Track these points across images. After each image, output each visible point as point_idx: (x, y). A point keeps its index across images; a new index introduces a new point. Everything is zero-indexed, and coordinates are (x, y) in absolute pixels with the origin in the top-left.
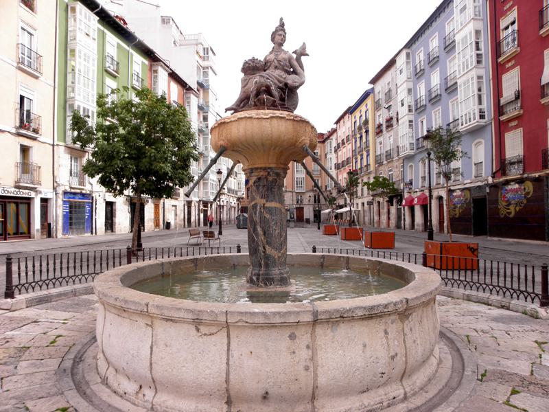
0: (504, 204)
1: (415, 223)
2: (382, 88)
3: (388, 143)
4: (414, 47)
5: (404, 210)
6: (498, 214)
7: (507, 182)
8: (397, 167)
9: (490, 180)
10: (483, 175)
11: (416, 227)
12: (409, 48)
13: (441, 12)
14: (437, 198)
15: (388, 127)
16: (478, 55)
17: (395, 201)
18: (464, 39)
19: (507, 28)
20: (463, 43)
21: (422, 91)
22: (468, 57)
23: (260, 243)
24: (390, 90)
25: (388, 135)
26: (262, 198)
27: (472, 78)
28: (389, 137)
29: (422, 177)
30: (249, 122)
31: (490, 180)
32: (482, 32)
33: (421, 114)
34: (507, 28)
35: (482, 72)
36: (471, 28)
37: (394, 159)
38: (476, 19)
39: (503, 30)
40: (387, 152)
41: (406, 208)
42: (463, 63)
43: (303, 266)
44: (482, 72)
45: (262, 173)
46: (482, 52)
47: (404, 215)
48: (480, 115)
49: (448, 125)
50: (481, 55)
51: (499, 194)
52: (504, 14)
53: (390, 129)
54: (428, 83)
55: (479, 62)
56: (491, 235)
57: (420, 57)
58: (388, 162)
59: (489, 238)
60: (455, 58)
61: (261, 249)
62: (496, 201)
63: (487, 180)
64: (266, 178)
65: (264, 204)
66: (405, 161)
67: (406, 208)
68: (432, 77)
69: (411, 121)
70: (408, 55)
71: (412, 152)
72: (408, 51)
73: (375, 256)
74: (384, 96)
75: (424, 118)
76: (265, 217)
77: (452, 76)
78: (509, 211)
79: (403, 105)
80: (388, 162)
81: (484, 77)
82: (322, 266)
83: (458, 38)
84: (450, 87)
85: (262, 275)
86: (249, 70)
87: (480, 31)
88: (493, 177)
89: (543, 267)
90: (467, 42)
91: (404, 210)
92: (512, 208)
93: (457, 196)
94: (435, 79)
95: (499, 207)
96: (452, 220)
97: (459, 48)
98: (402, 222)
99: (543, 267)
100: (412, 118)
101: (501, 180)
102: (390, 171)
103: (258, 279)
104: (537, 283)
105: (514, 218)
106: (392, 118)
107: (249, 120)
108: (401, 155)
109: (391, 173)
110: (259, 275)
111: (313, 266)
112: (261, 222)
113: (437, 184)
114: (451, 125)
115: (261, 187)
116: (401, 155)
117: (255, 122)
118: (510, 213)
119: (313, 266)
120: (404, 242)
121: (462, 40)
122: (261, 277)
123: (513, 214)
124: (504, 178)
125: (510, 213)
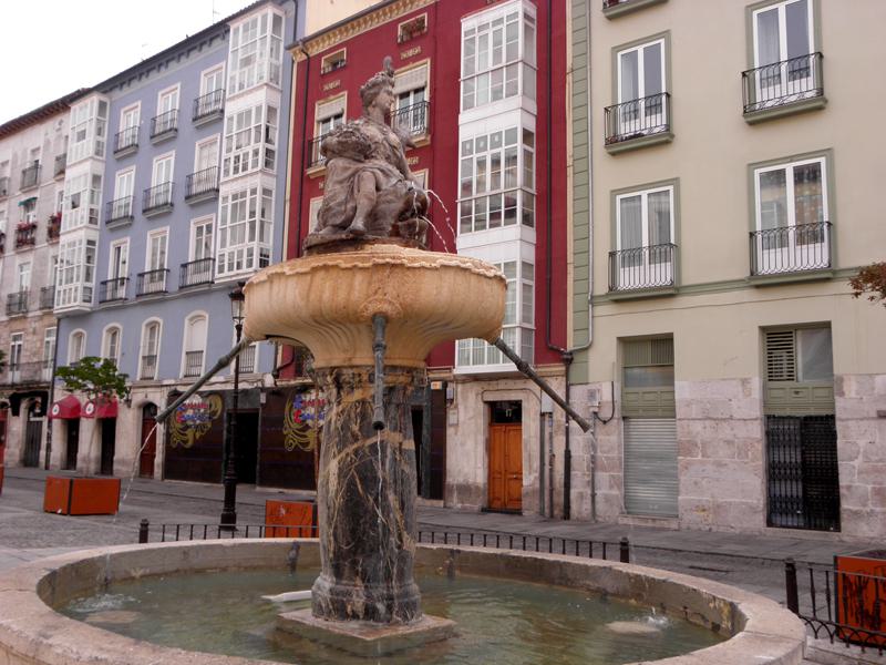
0: (295, 426)
1: (79, 456)
2: (15, 155)
3: (17, 277)
4: (117, 94)
5: (50, 426)
6: (282, 444)
7: (305, 389)
8: (34, 333)
9: (269, 381)
10: (255, 370)
11: (79, 464)
12: (105, 92)
13: (194, 48)
14: (140, 407)
15: (20, 243)
16: (269, 153)
17: (24, 405)
18: (244, 116)
19: (327, 120)
20: (239, 123)
21: (125, 186)
22: (250, 150)
23: (393, 528)
24: (36, 165)
25: (18, 260)
26: (395, 430)
27: (254, 192)
28: (21, 266)
29: (144, 358)
30: (460, 278)
31: (269, 381)
32: (278, 111)
33: (120, 233)
34: (327, 120)
35: (271, 183)
36: (260, 98)
37: (30, 315)
38: (271, 87)
39: (319, 122)
40: (11, 296)
41: (56, 422)
42: (237, 158)
43: (246, 568)
44: (271, 183)
45: (402, 379)
46: (275, 147)
47: (49, 437)
48: (261, 260)
49: (185, 266)
50: (273, 152)
51: (287, 409)
52: (324, 96)
53: (26, 248)
54: (144, 175)
55: (267, 164)
56: (262, 484)
57: (130, 121)
58: (12, 319)
59: (258, 489)
60: (213, 143)
61: (393, 539)
62: (280, 422)
63: (262, 381)
64: (405, 389)
65: (401, 444)
66: (63, 324)
67: (56, 422)
68: (155, 166)
69: (90, 242)
70: (102, 105)
71: (87, 307)
72: (104, 98)
73: (492, 546)
74: (19, 176)
75: (126, 243)
76: (403, 471)
77: (204, 175)
78: (184, 438)
79: (74, 206)
80: (12, 319)
81: (274, 192)
82: (293, 565)
83: (231, 109)
84: (196, 195)
85: (398, 597)
86: (354, 149)
87: (276, 110)
88: (276, 376)
89: (788, 565)
90: (248, 123)
91: (50, 426)
92: (190, 433)
93: (192, 406)
94: (163, 170)
95: (285, 432)
96: (172, 453)
97: (230, 127)
98: (43, 453)
99: (788, 565)
100: (94, 236)
101: (293, 382)
102: (15, 339)
103: (389, 608)
104: (822, 591)
105: (192, 448)
106: (34, 227)
107: (461, 273)
108: (59, 308)
109: (18, 343)
110: (391, 598)
111: (272, 568)
112: (395, 481)
113: (143, 379)
114: (190, 267)
115: (393, 406)
116: (59, 308)
117: (473, 279)
118: (186, 442)
119: (272, 568)
120: (13, 487)
121: (240, 116)
122: (396, 602)
123: (190, 443)
124: (299, 381)
125: (186, 442)
